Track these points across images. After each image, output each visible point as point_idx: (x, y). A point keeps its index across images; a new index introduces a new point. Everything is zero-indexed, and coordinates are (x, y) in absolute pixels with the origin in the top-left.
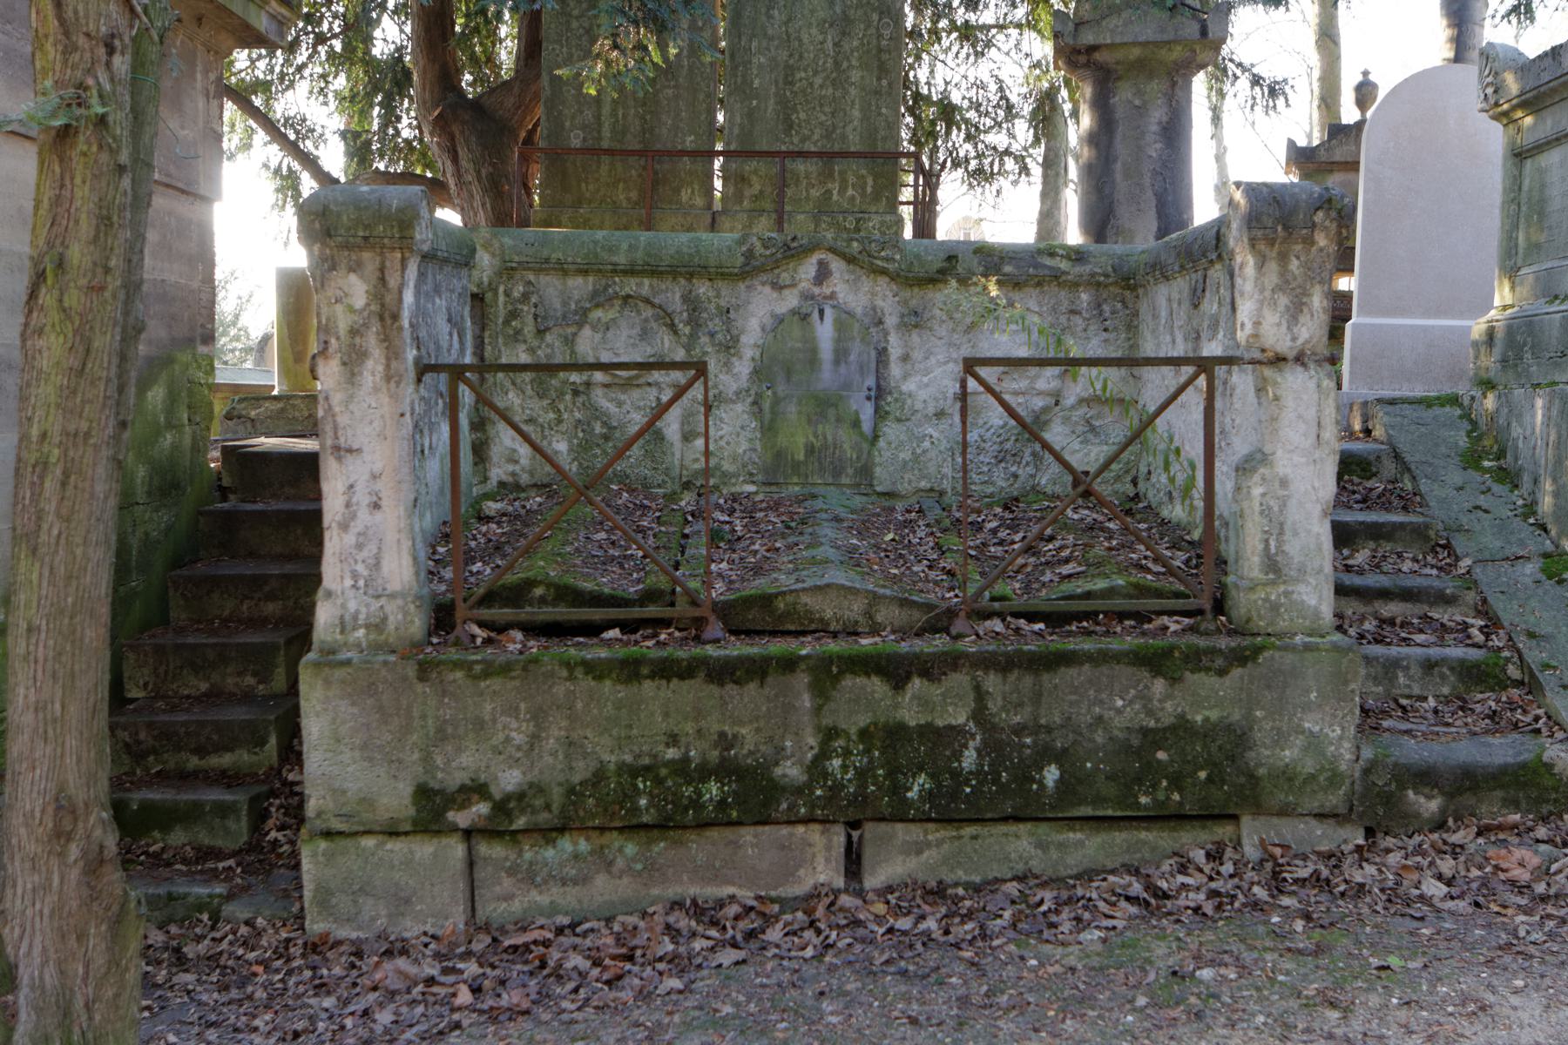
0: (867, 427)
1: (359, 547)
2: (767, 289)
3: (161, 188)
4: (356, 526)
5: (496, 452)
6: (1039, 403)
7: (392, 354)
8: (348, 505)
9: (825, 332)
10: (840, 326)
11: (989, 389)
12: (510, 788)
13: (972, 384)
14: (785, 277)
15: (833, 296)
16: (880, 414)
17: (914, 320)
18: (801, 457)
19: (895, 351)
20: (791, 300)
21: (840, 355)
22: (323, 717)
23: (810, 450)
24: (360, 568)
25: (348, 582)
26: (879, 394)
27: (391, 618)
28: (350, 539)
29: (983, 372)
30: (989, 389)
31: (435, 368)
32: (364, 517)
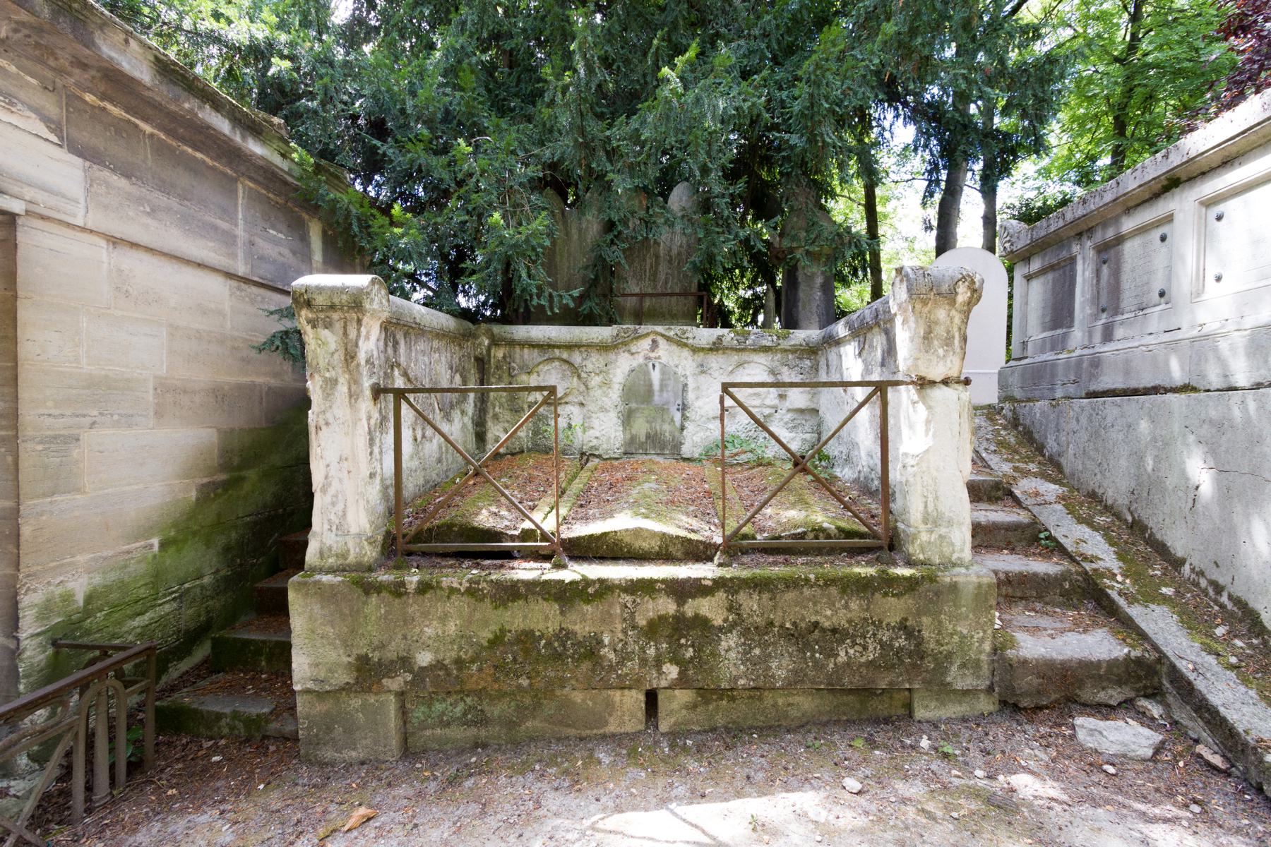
0: (678, 424)
1: (333, 504)
2: (626, 354)
3: (878, 412)
4: (332, 491)
5: (490, 436)
6: (767, 411)
7: (355, 381)
8: (326, 477)
9: (656, 376)
10: (663, 373)
11: (740, 404)
12: (424, 664)
13: (729, 402)
14: (634, 349)
15: (659, 358)
16: (684, 418)
17: (703, 370)
18: (643, 439)
19: (691, 386)
20: (640, 360)
21: (663, 387)
22: (304, 616)
23: (648, 436)
24: (333, 517)
25: (326, 527)
26: (684, 408)
27: (352, 551)
28: (328, 499)
29: (739, 393)
30: (740, 404)
31: (386, 391)
32: (335, 485)
